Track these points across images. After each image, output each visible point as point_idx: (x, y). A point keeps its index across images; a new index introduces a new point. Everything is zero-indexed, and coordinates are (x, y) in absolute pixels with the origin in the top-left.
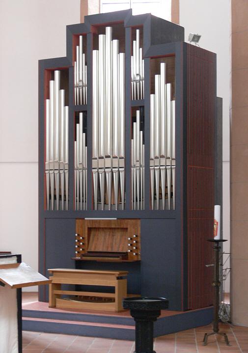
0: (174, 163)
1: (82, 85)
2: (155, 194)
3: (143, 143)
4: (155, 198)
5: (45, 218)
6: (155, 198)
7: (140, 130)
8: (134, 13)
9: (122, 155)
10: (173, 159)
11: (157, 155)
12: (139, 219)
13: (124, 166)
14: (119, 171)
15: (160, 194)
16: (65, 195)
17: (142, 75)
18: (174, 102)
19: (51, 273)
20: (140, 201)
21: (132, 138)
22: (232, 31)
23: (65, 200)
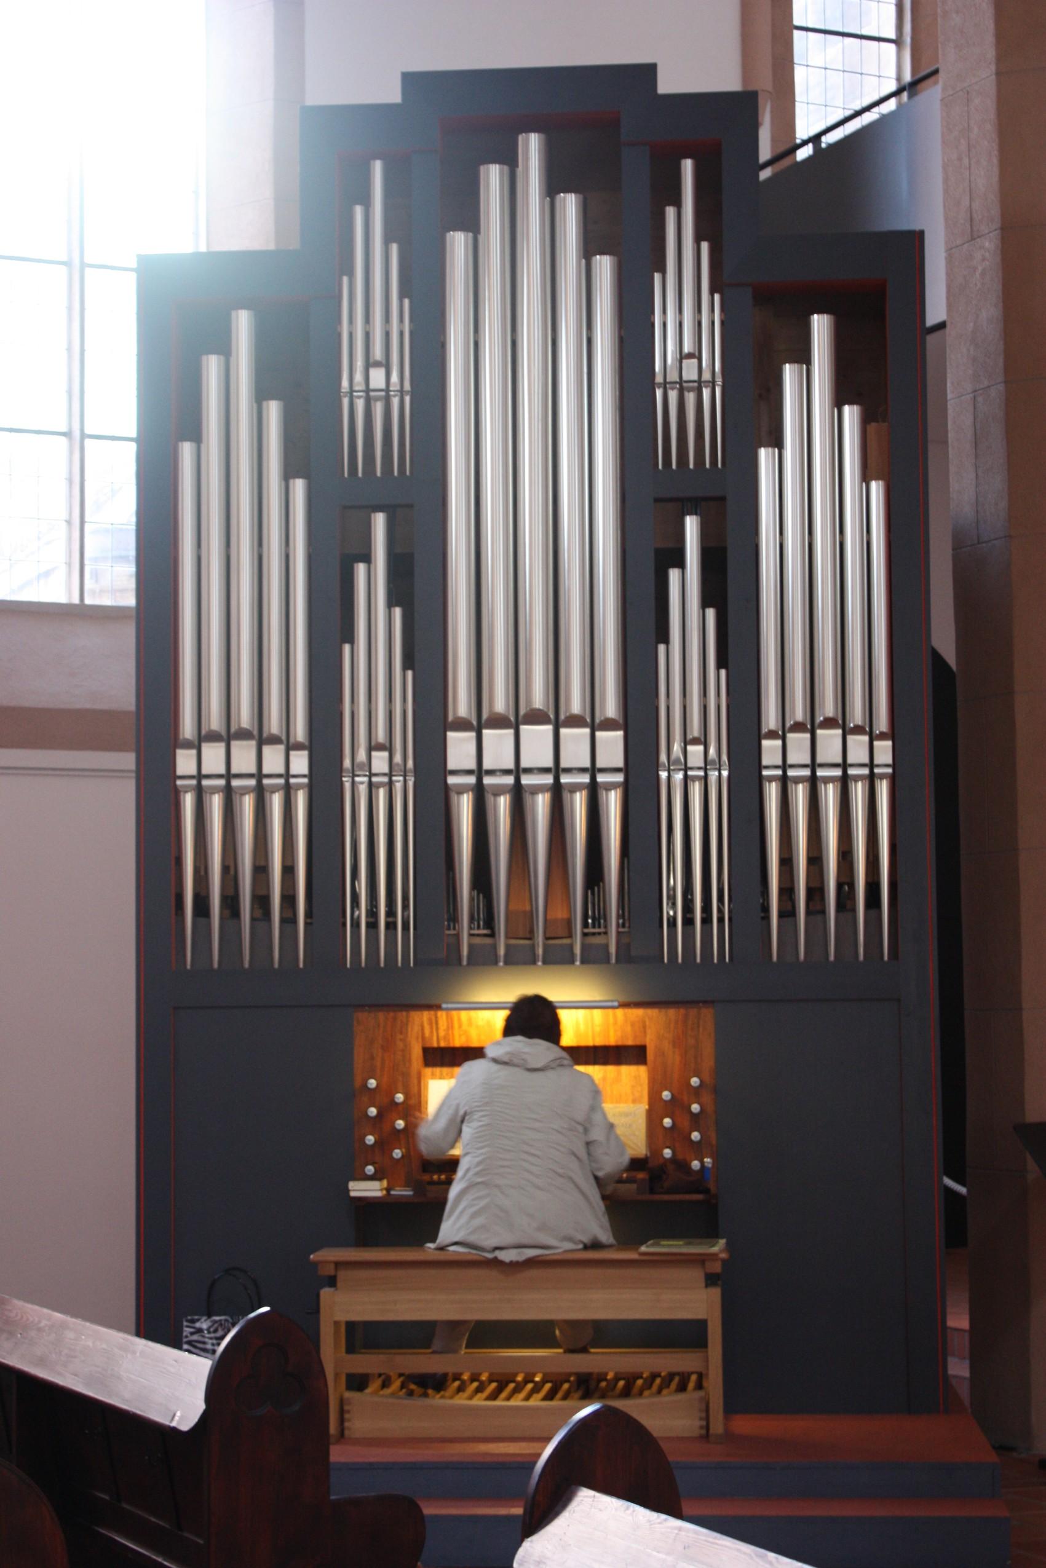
0: (884, 751)
1: (695, 377)
2: (787, 891)
3: (721, 663)
4: (788, 912)
5: (175, 1008)
6: (788, 912)
7: (705, 603)
8: (666, 86)
9: (610, 707)
10: (299, 747)
11: (215, 721)
12: (712, 1002)
13: (620, 763)
14: (199, 786)
15: (816, 892)
16: (289, 899)
17: (712, 360)
18: (876, 488)
19: (330, 1270)
20: (706, 920)
21: (663, 636)
22: (1003, 215)
23: (721, 920)
